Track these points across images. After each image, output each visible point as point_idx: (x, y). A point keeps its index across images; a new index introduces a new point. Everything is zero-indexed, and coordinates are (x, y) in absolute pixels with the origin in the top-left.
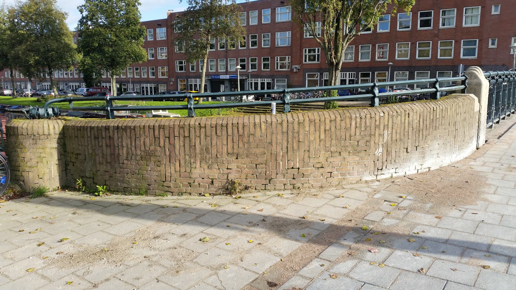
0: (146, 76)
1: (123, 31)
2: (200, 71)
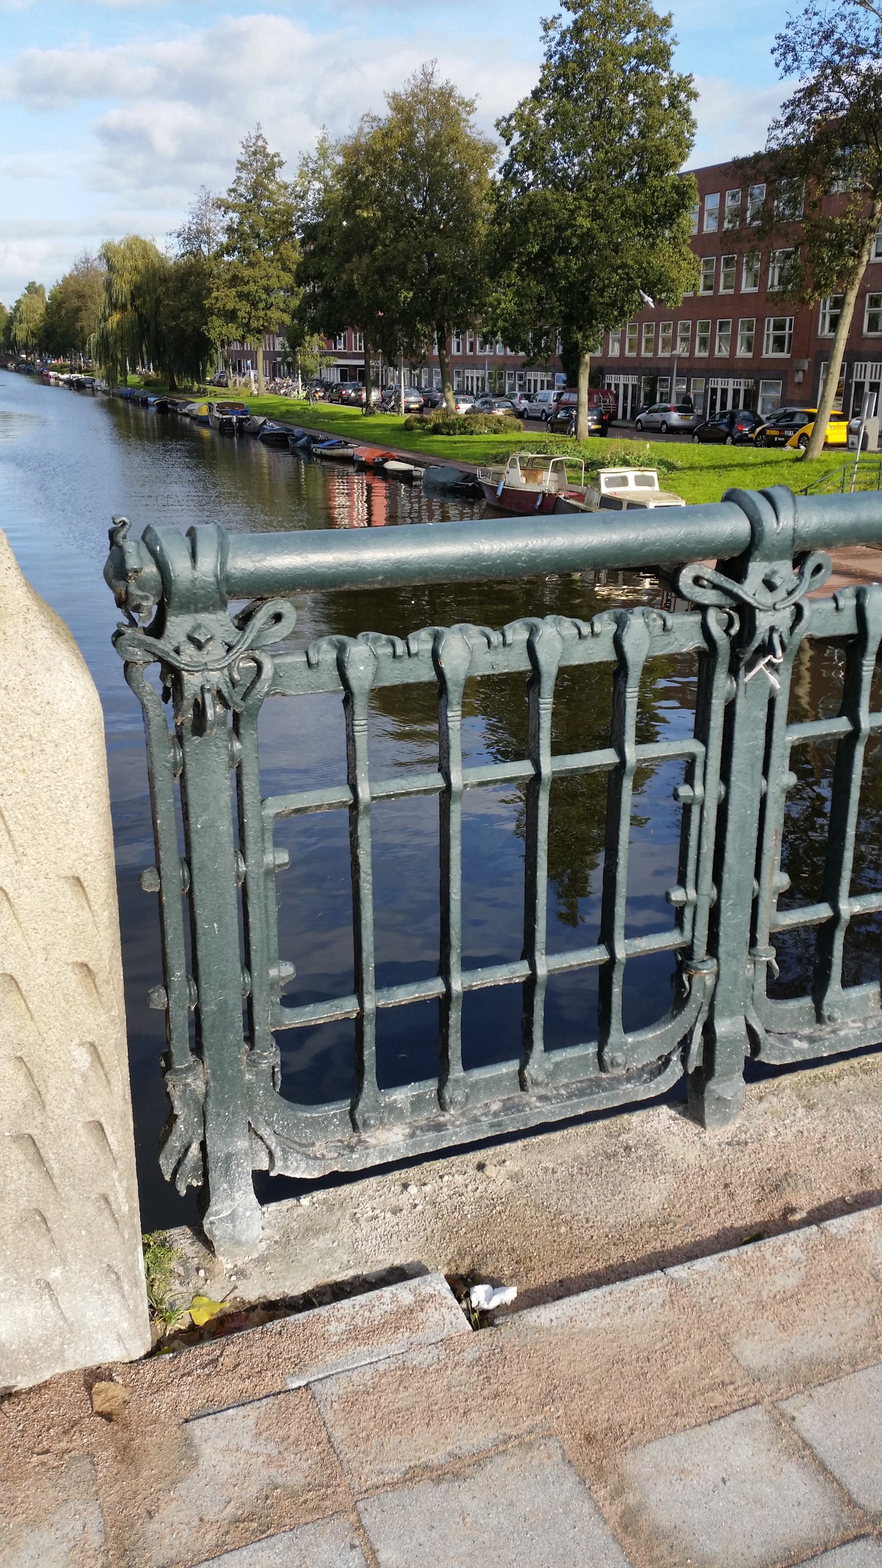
0: (725, 353)
1: (619, 197)
2: (825, 332)
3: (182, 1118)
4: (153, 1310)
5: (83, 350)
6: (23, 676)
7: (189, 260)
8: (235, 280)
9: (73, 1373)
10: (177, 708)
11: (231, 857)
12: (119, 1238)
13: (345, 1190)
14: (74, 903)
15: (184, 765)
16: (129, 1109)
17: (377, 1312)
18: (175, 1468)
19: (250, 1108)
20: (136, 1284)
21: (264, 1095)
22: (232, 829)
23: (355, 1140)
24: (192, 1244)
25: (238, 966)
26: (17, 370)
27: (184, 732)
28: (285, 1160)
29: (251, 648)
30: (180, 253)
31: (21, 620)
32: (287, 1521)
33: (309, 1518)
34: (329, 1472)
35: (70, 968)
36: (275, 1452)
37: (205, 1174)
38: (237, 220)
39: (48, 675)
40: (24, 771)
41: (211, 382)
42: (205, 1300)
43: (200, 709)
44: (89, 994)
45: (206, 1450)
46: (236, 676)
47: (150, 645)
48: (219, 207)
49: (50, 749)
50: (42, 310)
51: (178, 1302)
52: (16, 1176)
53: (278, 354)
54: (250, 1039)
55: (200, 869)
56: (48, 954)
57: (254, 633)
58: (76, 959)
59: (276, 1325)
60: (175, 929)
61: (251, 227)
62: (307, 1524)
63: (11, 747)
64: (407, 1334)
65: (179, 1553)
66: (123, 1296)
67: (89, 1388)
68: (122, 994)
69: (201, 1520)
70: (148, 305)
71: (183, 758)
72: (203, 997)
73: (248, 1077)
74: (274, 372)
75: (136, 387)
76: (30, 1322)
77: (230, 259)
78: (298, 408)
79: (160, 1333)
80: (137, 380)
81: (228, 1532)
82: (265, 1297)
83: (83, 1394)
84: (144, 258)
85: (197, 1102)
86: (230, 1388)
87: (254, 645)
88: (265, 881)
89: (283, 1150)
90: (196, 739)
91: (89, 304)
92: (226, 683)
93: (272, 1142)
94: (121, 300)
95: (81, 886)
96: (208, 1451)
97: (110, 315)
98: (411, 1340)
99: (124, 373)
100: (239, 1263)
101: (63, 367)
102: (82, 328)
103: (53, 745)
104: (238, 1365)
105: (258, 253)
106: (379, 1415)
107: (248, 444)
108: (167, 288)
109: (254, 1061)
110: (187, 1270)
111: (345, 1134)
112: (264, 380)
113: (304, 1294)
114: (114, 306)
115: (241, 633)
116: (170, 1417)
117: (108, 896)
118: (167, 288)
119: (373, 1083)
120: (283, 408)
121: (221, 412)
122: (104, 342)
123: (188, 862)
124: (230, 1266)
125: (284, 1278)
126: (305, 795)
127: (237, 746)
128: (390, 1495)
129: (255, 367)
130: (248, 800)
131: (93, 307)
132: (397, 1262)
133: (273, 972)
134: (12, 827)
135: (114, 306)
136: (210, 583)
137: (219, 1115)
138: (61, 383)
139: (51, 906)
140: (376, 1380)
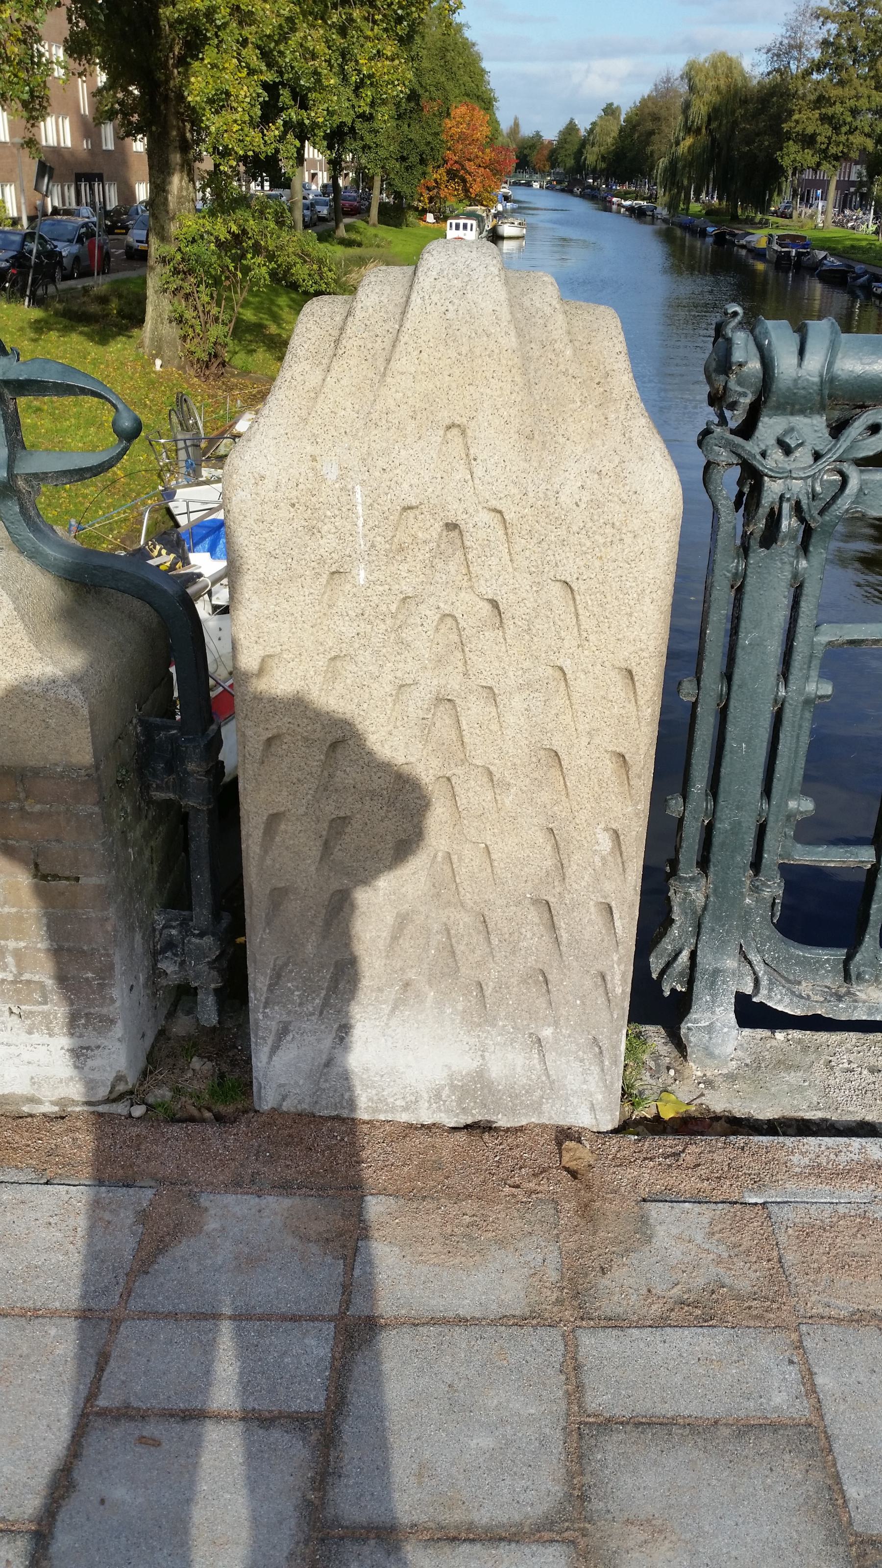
3: (678, 924)
4: (626, 1094)
5: (650, 175)
6: (617, 462)
7: (775, 78)
8: (821, 101)
9: (547, 1126)
10: (749, 518)
11: (773, 680)
12: (609, 1017)
13: (822, 1037)
14: (623, 694)
15: (745, 576)
16: (637, 899)
17: (842, 1158)
18: (629, 1238)
19: (745, 932)
20: (615, 1062)
21: (761, 922)
22: (779, 651)
23: (843, 990)
24: (665, 1044)
25: (758, 790)
26: (582, 196)
27: (752, 542)
28: (770, 990)
29: (840, 460)
30: (766, 71)
31: (623, 407)
32: (731, 1319)
33: (752, 1323)
34: (776, 1288)
35: (608, 756)
36: (725, 1255)
37: (691, 982)
38: (834, 32)
39: (640, 464)
40: (601, 558)
41: (775, 212)
42: (673, 1097)
43: (774, 519)
44: (621, 784)
45: (661, 1232)
46: (818, 489)
47: (738, 446)
48: (817, 17)
49: (628, 539)
50: (615, 133)
51: (646, 1092)
52: (529, 935)
53: (853, 184)
54: (756, 865)
55: (740, 687)
56: (591, 738)
57: (848, 443)
58: (614, 749)
59: (740, 1140)
60: (704, 742)
61: (849, 40)
62: (749, 1327)
63: (594, 533)
64: (872, 1187)
65: (626, 1312)
66: (603, 1070)
67: (559, 1144)
68: (649, 791)
69: (649, 1291)
70: (723, 129)
71: (746, 569)
72: (718, 814)
73: (748, 901)
74: (844, 203)
75: (697, 216)
76: (519, 1069)
77: (819, 77)
78: (864, 243)
79: (627, 1115)
80: (699, 209)
81: (673, 1310)
82: (730, 1112)
83: (553, 1146)
84: (727, 77)
85: (695, 913)
86: (690, 1184)
87: (845, 456)
88: (803, 710)
89: (770, 980)
90: (763, 552)
91: (663, 127)
92: (808, 493)
93: (761, 969)
94: (698, 122)
95: (632, 679)
96: (662, 1233)
97: (684, 139)
98: (876, 1193)
99: (687, 200)
100: (708, 1074)
101: (627, 193)
102: (652, 152)
103: (632, 535)
104: (699, 1165)
105: (852, 70)
106: (833, 1252)
107: (804, 279)
108: (746, 110)
109: (757, 887)
110: (658, 1065)
111: (834, 982)
112: (832, 211)
113: (769, 1120)
114: (688, 129)
115: (833, 442)
116: (630, 1192)
117: (654, 693)
118: (746, 110)
119: (875, 939)
120: (848, 243)
121: (780, 245)
122: (672, 169)
123: (728, 676)
124: (699, 1074)
125: (752, 1100)
126: (864, 627)
127: (803, 564)
128: (834, 1329)
129: (824, 197)
130: (802, 622)
131: (666, 130)
132: (869, 1118)
133: (792, 804)
134: (581, 611)
135: (688, 129)
136: (813, 383)
137: (713, 930)
138: (623, 210)
139: (602, 693)
140: (835, 1220)
